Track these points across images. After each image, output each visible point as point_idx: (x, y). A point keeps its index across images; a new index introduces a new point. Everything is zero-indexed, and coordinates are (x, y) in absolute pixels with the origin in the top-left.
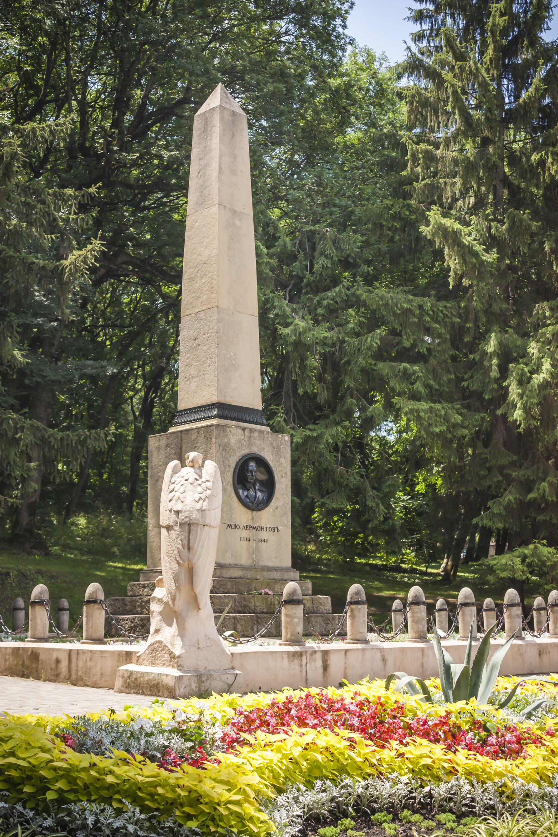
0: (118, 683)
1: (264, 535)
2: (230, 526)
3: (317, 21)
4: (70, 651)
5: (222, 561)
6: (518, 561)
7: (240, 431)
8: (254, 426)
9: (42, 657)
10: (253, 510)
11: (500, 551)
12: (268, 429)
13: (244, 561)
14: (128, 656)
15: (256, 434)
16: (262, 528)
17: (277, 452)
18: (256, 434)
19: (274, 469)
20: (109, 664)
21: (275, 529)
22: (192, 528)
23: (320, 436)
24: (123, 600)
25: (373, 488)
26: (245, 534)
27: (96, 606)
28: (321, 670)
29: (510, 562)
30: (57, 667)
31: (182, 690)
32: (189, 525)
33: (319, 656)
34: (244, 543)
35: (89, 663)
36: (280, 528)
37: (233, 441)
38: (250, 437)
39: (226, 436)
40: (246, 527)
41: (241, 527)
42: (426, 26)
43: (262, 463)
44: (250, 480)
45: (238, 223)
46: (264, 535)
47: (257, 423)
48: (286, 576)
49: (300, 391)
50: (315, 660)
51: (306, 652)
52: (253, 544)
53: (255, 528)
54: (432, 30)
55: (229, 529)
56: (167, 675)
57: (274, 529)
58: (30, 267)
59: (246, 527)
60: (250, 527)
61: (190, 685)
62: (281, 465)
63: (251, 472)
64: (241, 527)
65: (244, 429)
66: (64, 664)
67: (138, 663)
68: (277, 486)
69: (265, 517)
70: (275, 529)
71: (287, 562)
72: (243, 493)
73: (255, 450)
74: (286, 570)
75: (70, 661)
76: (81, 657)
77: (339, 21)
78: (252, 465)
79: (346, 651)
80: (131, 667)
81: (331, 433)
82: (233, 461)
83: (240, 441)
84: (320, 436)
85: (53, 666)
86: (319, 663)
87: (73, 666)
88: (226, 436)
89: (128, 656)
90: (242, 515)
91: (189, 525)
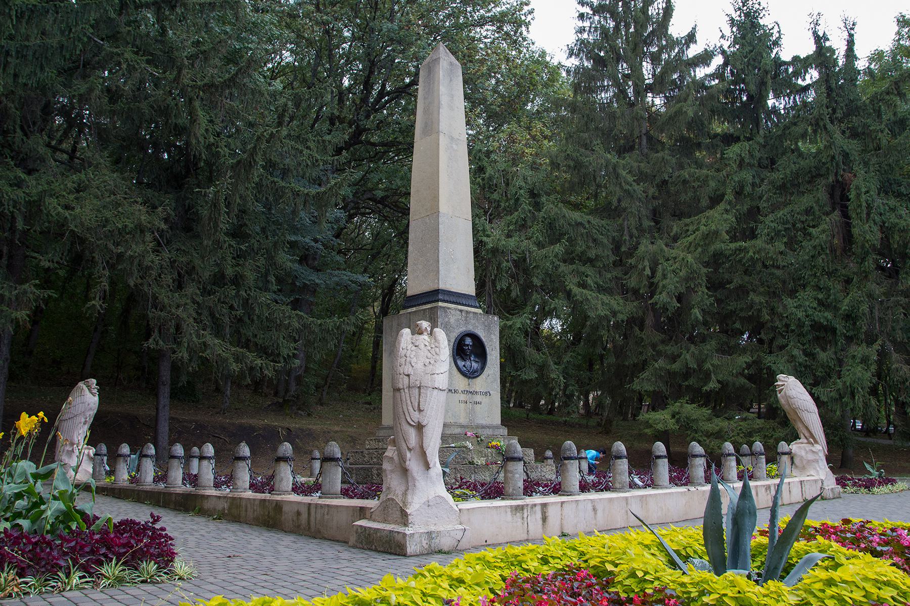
0: (353, 539)
1: (478, 398)
3: (507, 28)
4: (310, 504)
5: (448, 421)
6: (668, 417)
8: (469, 309)
9: (286, 508)
10: (469, 378)
11: (654, 408)
13: (463, 420)
14: (362, 512)
15: (471, 315)
16: (476, 392)
17: (488, 328)
18: (471, 315)
19: (486, 344)
20: (343, 518)
21: (487, 393)
22: (422, 391)
23: (514, 324)
25: (556, 364)
26: (463, 397)
27: (333, 463)
28: (540, 522)
29: (662, 418)
30: (298, 519)
31: (413, 547)
32: (419, 388)
33: (538, 509)
34: (463, 405)
35: (326, 517)
37: (452, 320)
38: (467, 317)
39: (446, 316)
42: (587, 24)
43: (475, 338)
44: (468, 350)
45: (454, 146)
46: (478, 398)
47: (471, 306)
48: (497, 432)
49: (498, 288)
50: (535, 513)
51: (527, 505)
52: (470, 406)
54: (590, 27)
55: (450, 394)
56: (398, 533)
58: (297, 194)
61: (421, 542)
62: (491, 340)
65: (461, 311)
66: (304, 516)
67: (370, 519)
68: (489, 357)
69: (479, 384)
70: (487, 393)
71: (497, 420)
72: (461, 363)
73: (471, 328)
74: (497, 427)
75: (309, 514)
76: (319, 511)
77: (524, 28)
78: (468, 341)
79: (562, 503)
80: (363, 523)
81: (520, 321)
82: (455, 335)
83: (458, 320)
84: (514, 324)
85: (295, 518)
86: (539, 515)
87: (312, 519)
88: (446, 316)
89: (362, 512)
90: (461, 383)
91: (419, 388)
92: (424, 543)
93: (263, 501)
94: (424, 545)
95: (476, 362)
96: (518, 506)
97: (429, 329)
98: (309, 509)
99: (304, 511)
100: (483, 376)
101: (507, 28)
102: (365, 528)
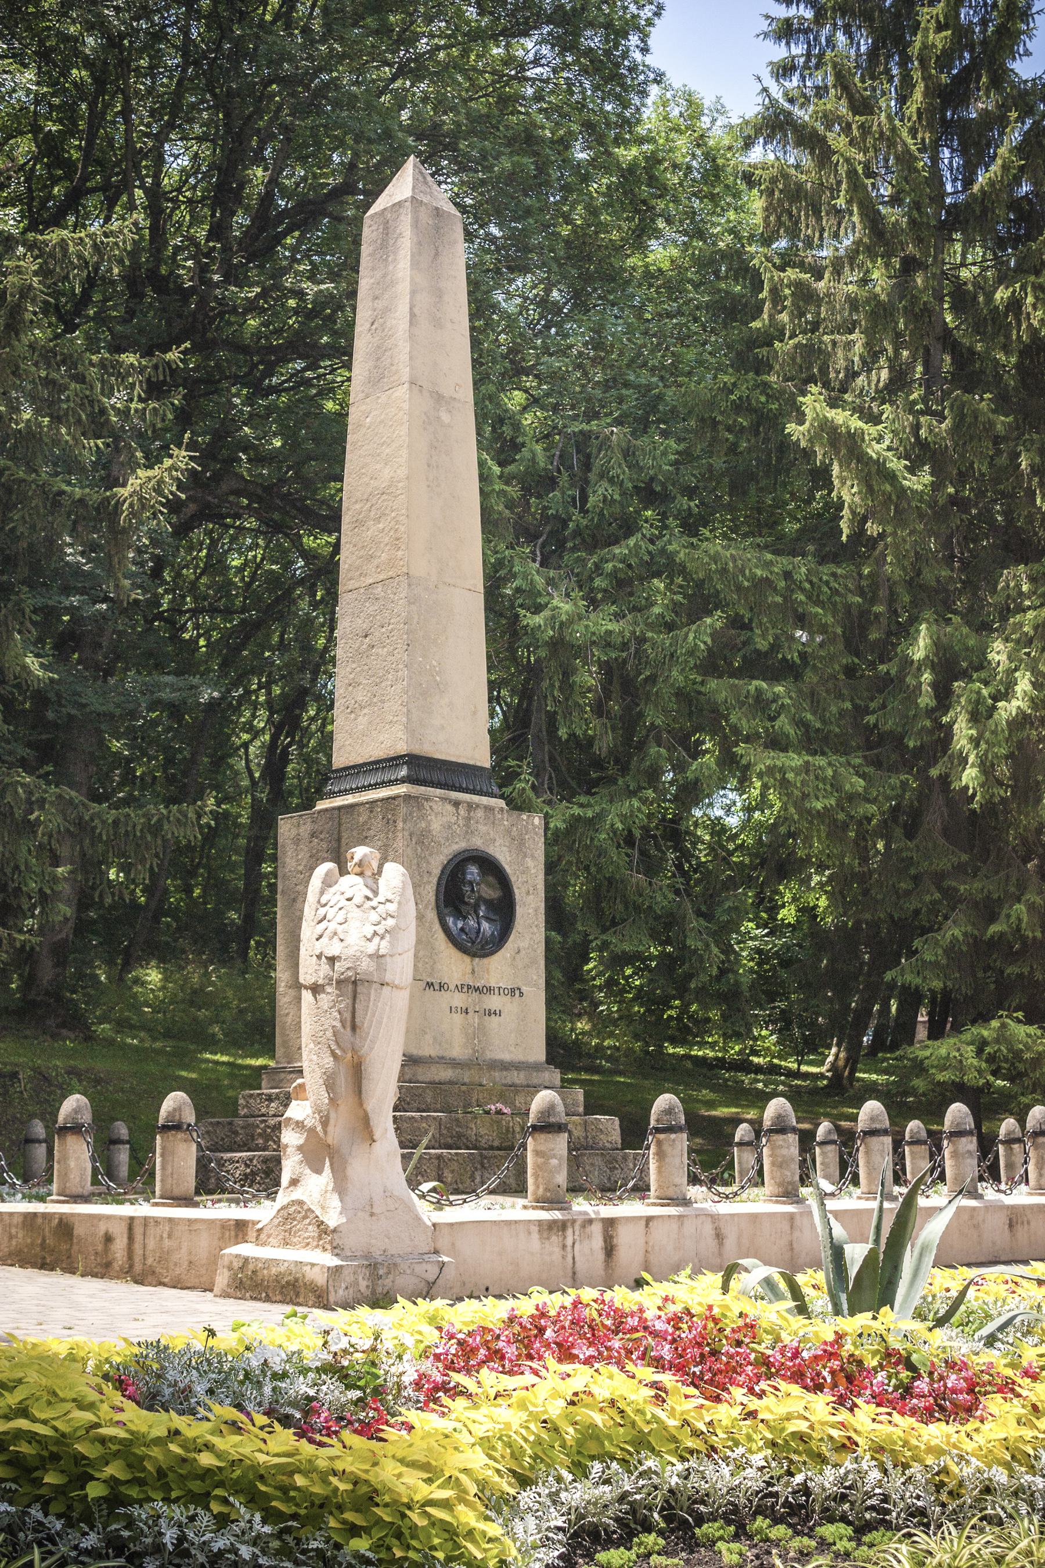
0: (222, 1279)
1: (494, 1002)
2: (430, 985)
3: (593, 40)
4: (132, 1219)
5: (415, 1052)
6: (970, 1051)
7: (450, 808)
8: (476, 798)
9: (79, 1230)
10: (473, 955)
11: (936, 1032)
12: (502, 803)
13: (458, 1050)
14: (240, 1229)
15: (480, 813)
16: (490, 990)
17: (519, 845)
18: (480, 813)
19: (513, 879)
21: (514, 992)
22: (360, 989)
24: (230, 1123)
25: (699, 914)
26: (459, 1000)
27: (180, 1135)
28: (601, 1256)
29: (954, 1053)
30: (106, 1250)
31: (341, 1292)
32: (355, 983)
33: (597, 1229)
34: (458, 1018)
35: (167, 1243)
36: (524, 989)
37: (436, 826)
38: (468, 819)
39: (423, 817)
40: (460, 988)
41: (452, 987)
43: (490, 866)
44: (467, 900)
45: (445, 417)
46: (494, 1002)
47: (481, 793)
48: (536, 1078)
49: (563, 733)
51: (574, 1221)
52: (474, 1019)
53: (477, 989)
54: (808, 55)
55: (429, 992)
56: (313, 1265)
57: (513, 990)
58: (55, 500)
59: (460, 988)
60: (469, 987)
63: (471, 883)
64: (452, 987)
65: (456, 804)
68: (519, 911)
69: (497, 968)
70: (514, 992)
71: (538, 1052)
72: (455, 924)
74: (535, 1067)
76: (152, 1231)
77: (634, 40)
78: (473, 872)
79: (649, 1220)
80: (246, 1249)
81: (619, 812)
82: (437, 863)
83: (449, 826)
84: (600, 816)
86: (597, 1242)
88: (423, 817)
89: (240, 1229)
90: (454, 966)
92: (363, 1284)
93: (30, 1218)
94: (363, 1289)
95: (488, 919)
96: (555, 1222)
97: (375, 865)
98: (130, 1229)
99: (120, 1234)
100: (506, 952)
101: (593, 40)
102: (246, 1260)
